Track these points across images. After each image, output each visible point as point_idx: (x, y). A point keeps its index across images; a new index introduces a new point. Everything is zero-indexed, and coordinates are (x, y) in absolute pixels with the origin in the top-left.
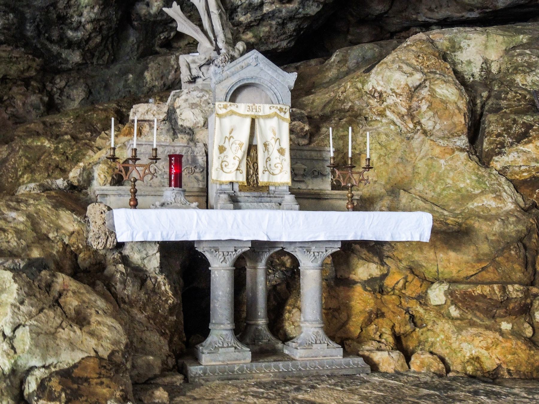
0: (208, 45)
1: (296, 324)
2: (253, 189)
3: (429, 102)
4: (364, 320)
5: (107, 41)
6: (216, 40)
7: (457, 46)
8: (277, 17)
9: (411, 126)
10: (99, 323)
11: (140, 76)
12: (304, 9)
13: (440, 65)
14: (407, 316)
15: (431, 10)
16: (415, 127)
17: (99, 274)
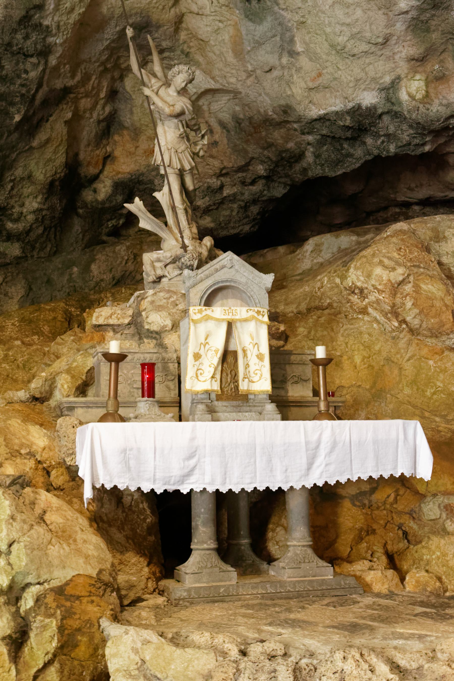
0: (174, 242)
1: (281, 544)
2: (230, 397)
3: (414, 298)
4: (354, 538)
5: (49, 232)
6: (182, 237)
7: (441, 236)
8: (239, 200)
9: (396, 324)
10: (85, 541)
11: (86, 269)
12: (268, 190)
13: (424, 258)
14: (400, 532)
15: (412, 190)
16: (400, 325)
17: (75, 491)
